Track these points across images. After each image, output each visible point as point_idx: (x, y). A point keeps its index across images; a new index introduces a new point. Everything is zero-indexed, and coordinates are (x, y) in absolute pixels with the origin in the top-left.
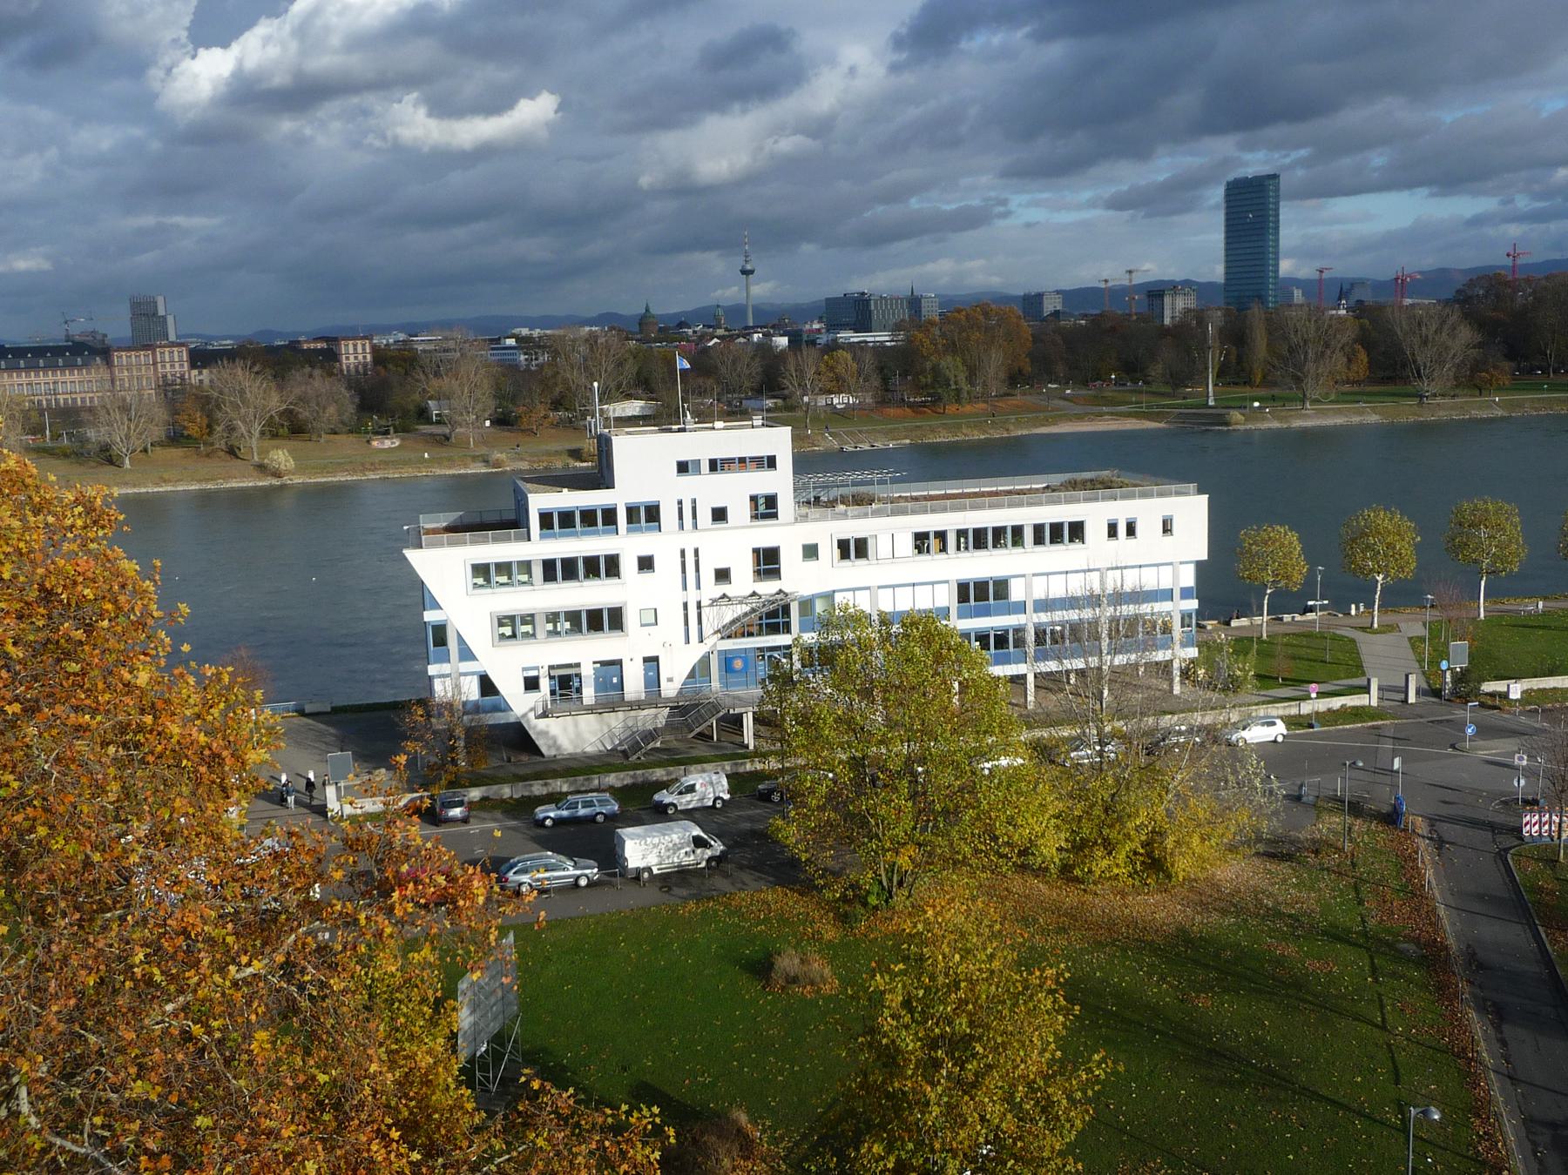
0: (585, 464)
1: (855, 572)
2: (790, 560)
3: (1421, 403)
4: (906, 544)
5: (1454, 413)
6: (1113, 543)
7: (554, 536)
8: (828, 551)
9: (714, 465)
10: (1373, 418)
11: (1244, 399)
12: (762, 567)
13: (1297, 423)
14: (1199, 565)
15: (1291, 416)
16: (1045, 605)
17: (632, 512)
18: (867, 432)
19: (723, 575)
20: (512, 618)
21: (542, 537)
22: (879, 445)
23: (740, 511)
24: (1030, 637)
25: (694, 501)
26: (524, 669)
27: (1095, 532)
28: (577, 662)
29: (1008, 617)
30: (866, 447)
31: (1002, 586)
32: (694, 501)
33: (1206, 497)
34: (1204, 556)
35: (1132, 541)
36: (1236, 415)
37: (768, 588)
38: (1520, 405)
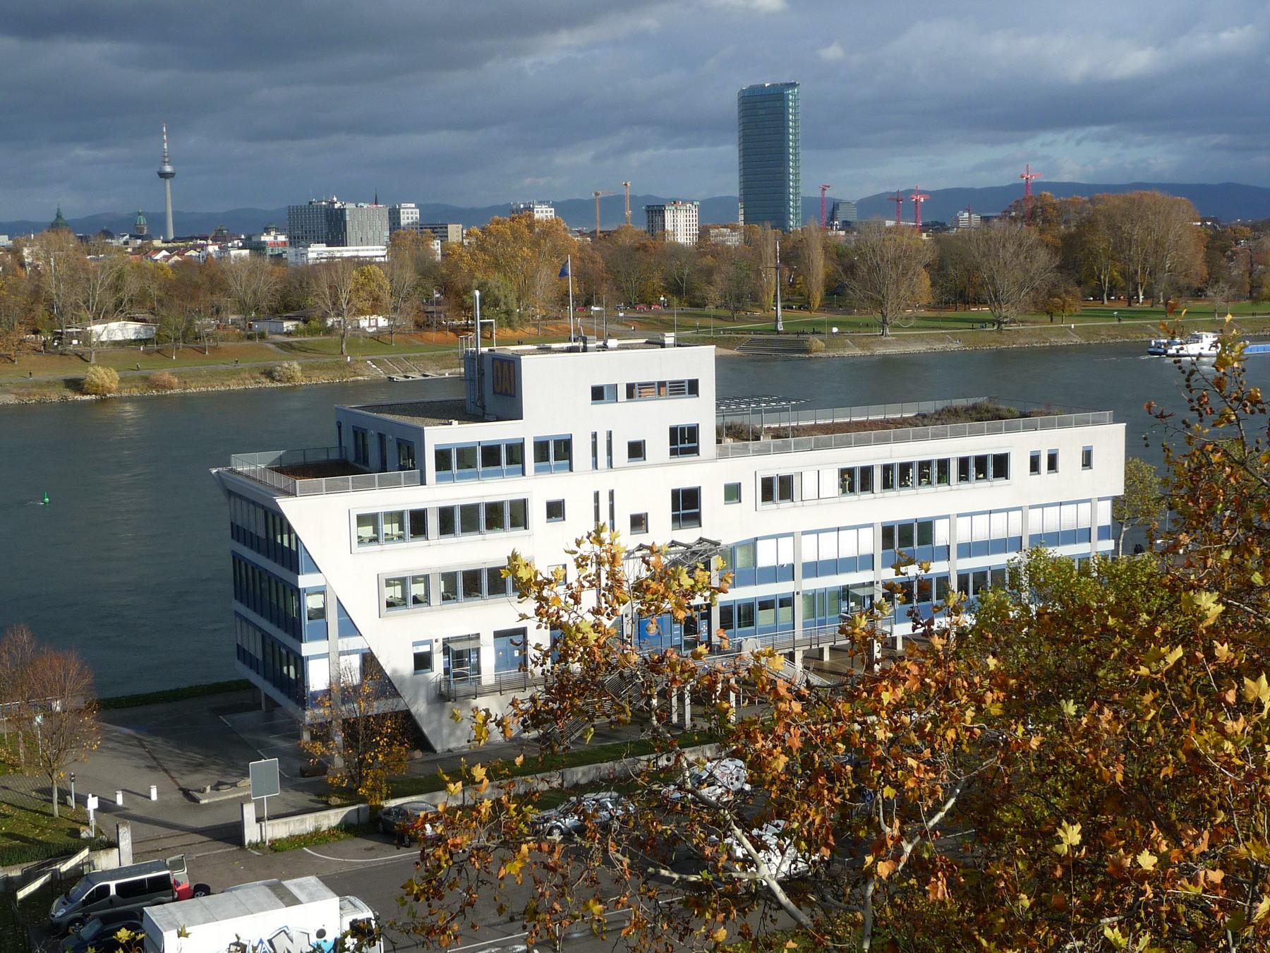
0: (87, 397)
1: (780, 515)
2: (711, 503)
3: (1000, 330)
4: (831, 482)
5: (1034, 340)
6: (1036, 477)
7: (452, 478)
8: (751, 491)
9: (631, 391)
10: (955, 346)
11: (821, 323)
12: (682, 512)
13: (880, 351)
14: (1116, 500)
15: (872, 342)
16: (968, 550)
17: (542, 449)
18: (415, 358)
19: (638, 522)
20: (402, 581)
21: (439, 479)
22: (432, 374)
23: (658, 446)
24: (954, 584)
25: (610, 434)
26: (415, 644)
27: (1018, 465)
28: (472, 632)
29: (968, 559)
30: (418, 377)
31: (926, 528)
32: (610, 434)
33: (1122, 427)
34: (1119, 490)
35: (1053, 476)
36: (816, 342)
37: (688, 536)
38: (1096, 331)
